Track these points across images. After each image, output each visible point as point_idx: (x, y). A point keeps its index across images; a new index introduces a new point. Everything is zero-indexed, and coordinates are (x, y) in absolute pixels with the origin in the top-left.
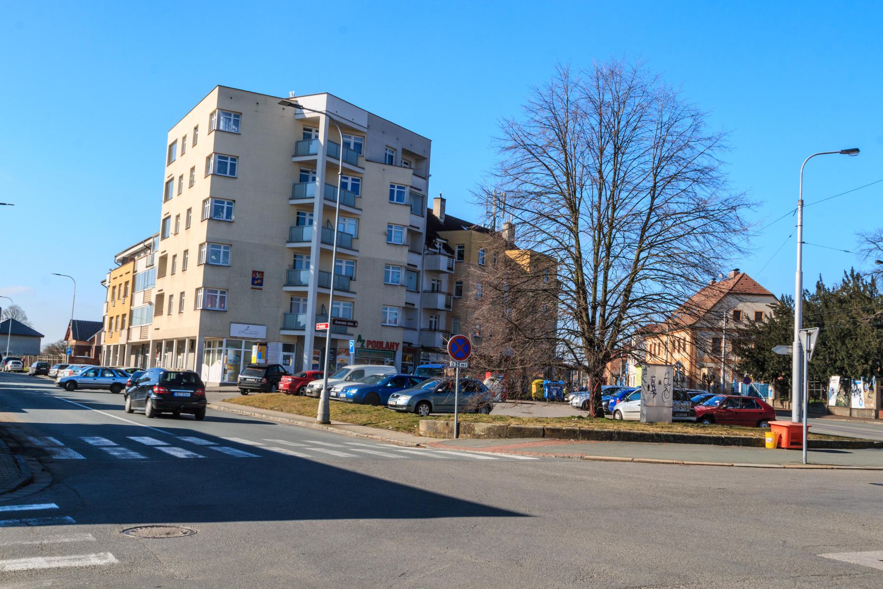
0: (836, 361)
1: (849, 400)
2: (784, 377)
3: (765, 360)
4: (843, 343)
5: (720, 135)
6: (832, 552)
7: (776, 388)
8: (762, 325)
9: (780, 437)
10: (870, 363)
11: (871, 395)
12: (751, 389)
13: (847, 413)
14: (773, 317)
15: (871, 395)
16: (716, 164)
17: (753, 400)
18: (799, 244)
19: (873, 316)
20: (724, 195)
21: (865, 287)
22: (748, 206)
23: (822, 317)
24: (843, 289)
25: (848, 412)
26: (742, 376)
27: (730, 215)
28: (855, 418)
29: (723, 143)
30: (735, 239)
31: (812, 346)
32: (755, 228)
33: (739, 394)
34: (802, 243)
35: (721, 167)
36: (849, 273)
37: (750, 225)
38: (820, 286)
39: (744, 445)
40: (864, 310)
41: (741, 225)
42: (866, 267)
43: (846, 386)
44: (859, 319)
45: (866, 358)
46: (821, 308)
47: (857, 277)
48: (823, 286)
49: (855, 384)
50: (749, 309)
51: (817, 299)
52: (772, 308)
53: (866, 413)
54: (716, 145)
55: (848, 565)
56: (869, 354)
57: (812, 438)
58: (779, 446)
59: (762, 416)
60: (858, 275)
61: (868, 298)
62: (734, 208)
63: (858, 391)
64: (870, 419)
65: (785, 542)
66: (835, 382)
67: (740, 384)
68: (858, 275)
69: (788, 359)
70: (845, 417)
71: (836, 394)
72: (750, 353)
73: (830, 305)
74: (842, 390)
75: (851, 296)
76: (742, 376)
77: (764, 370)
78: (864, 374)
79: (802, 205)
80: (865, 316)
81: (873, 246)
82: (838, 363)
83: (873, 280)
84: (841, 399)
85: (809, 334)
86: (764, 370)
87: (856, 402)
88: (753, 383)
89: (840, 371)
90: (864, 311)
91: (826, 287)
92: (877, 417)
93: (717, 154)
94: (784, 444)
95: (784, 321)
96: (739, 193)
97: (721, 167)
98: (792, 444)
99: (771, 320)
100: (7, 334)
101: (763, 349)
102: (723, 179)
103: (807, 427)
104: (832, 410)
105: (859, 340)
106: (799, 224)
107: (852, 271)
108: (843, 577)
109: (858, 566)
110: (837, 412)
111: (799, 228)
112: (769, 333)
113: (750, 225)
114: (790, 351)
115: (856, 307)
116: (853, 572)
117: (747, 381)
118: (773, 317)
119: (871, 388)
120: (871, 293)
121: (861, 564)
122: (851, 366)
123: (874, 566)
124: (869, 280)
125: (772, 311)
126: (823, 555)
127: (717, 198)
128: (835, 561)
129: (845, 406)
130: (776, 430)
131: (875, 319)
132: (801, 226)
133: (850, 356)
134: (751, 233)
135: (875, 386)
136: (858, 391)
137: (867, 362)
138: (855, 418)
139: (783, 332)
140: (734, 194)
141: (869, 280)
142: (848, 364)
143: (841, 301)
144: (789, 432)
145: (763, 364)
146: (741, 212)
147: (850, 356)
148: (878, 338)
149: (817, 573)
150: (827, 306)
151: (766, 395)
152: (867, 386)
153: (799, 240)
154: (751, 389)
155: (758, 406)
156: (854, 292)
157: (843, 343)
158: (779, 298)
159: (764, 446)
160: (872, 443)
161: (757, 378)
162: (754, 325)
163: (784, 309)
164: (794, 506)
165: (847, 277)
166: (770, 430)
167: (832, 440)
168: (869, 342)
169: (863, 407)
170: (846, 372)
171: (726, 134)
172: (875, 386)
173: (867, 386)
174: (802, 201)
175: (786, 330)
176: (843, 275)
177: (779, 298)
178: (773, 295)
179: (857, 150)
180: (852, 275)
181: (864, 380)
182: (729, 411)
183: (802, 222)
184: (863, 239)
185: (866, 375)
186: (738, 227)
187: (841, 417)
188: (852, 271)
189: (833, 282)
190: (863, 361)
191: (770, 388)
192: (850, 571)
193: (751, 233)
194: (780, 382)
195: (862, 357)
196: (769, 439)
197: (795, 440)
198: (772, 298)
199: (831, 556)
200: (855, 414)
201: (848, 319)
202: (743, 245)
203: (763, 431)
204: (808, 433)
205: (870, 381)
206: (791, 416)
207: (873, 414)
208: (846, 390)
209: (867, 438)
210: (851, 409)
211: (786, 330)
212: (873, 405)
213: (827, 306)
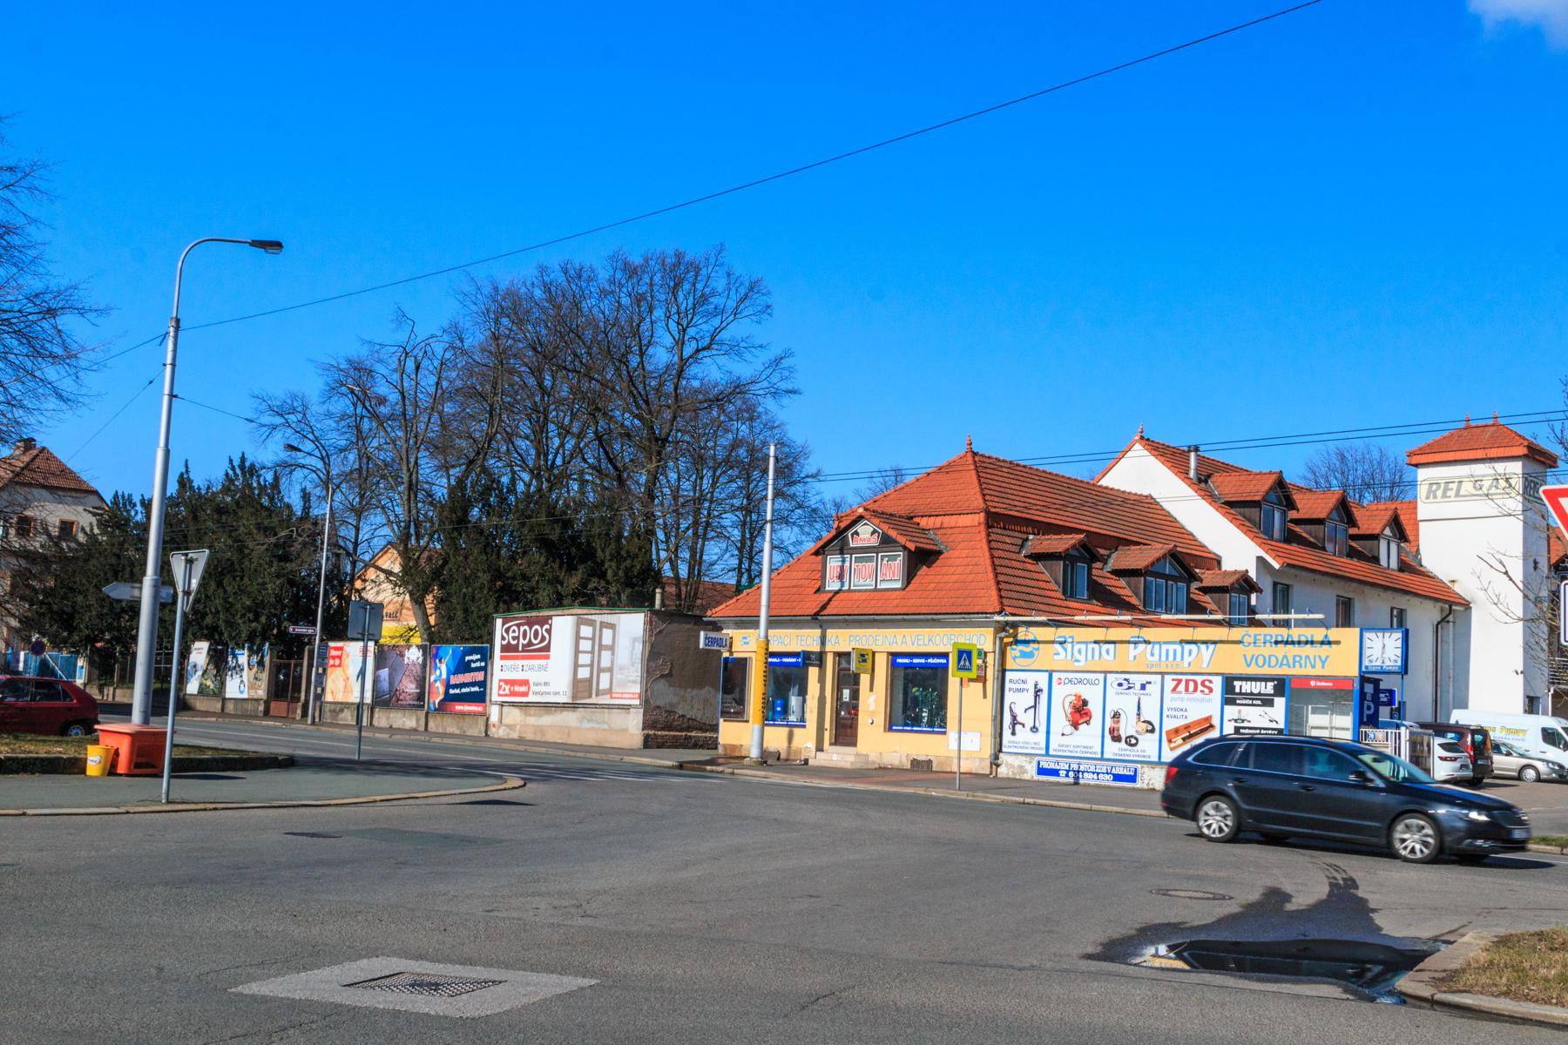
0: (204, 615)
1: (223, 684)
2: (108, 641)
3: (75, 611)
4: (220, 584)
5: (33, 166)
6: (254, 979)
7: (91, 663)
8: (73, 545)
9: (117, 753)
10: (263, 619)
11: (260, 675)
12: (44, 667)
13: (216, 706)
14: (96, 531)
15: (260, 675)
16: (21, 221)
17: (47, 683)
18: (166, 399)
19: (273, 540)
20: (36, 285)
21: (262, 488)
22: (82, 312)
23: (185, 536)
24: (226, 489)
25: (219, 706)
26: (27, 640)
27: (45, 324)
28: (230, 716)
29: (43, 185)
30: (51, 372)
31: (195, 583)
32: (92, 356)
33: (19, 673)
34: (172, 396)
35: (31, 229)
36: (236, 463)
37: (83, 349)
38: (184, 482)
39: (44, 772)
40: (259, 527)
41: (65, 348)
42: (267, 454)
43: (219, 662)
44: (251, 545)
45: (256, 610)
46: (191, 516)
47: (250, 471)
48: (191, 482)
49: (235, 656)
50: (52, 513)
51: (178, 505)
52: (95, 515)
53: (250, 706)
54: (23, 183)
55: (292, 1005)
56: (262, 605)
57: (181, 754)
58: (111, 770)
59: (81, 717)
60: (252, 465)
61: (267, 509)
62: (51, 312)
63: (238, 668)
64: (256, 717)
65: (160, 969)
66: (200, 653)
67: (22, 654)
68: (252, 465)
69: (134, 609)
70: (213, 714)
71: (200, 673)
72: (46, 596)
73: (201, 514)
74: (211, 667)
75: (237, 503)
76: (27, 640)
77: (71, 629)
78: (251, 639)
79: (177, 329)
80: (260, 538)
81: (278, 420)
82: (209, 620)
83: (276, 478)
84: (209, 683)
85: (190, 562)
86: (71, 629)
87: (235, 688)
88: (46, 655)
89: (211, 634)
90: (259, 529)
91: (195, 485)
92: (267, 712)
93: (24, 202)
94: (122, 767)
95: (115, 541)
96: (65, 283)
97: (31, 229)
98: (138, 766)
99: (91, 537)
100: (160, 775)
101: (72, 590)
102: (32, 253)
103: (173, 732)
104: (191, 701)
105: (246, 580)
106: (169, 361)
107: (243, 459)
108: (291, 1032)
109: (310, 1003)
110: (200, 705)
111: (169, 368)
112: (86, 561)
113: (83, 349)
114: (136, 593)
115: (246, 522)
116: (304, 1018)
117: (37, 649)
118: (96, 531)
119: (261, 663)
120: (272, 499)
121: (315, 998)
122: (230, 624)
123: (338, 999)
124: (269, 477)
125: (94, 520)
126: (240, 988)
127: (19, 287)
128: (265, 1000)
129: (215, 694)
130: (109, 742)
131: (276, 545)
132: (173, 365)
133: (228, 608)
134: (83, 364)
135: (267, 659)
136: (238, 668)
137: (257, 619)
138: (230, 716)
139: (113, 561)
140: (53, 284)
141: (269, 477)
142: (226, 622)
143: (221, 510)
144: (132, 745)
145: (71, 616)
146: (66, 321)
147: (228, 608)
148: (278, 577)
149: (239, 1031)
150: (195, 518)
151: (72, 672)
152: (255, 659)
153: (167, 391)
154: (44, 663)
155: (66, 695)
156: (243, 497)
157: (220, 584)
158: (108, 498)
159: (83, 771)
160: (276, 759)
161: (57, 644)
162: (57, 544)
163: (119, 520)
164: (159, 889)
165: (233, 468)
166: (96, 742)
167: (208, 755)
168: (265, 583)
169: (245, 696)
170: (221, 634)
171: (45, 166)
172: (267, 659)
173: (255, 659)
174: (178, 321)
175: (118, 556)
176: (227, 465)
177: (108, 498)
178: (95, 493)
179: (278, 245)
180: (242, 466)
181: (250, 649)
182: (11, 705)
183: (174, 358)
184: (264, 407)
185: (253, 643)
186: (58, 350)
187: (207, 714)
188: (243, 459)
189: (209, 474)
190: (251, 616)
191: (81, 662)
192: (296, 1013)
193: (83, 364)
194: (99, 650)
195: (249, 609)
196: (94, 758)
197: (145, 758)
198: (93, 498)
199: (255, 988)
200: (230, 707)
201: (230, 542)
202: (67, 385)
203: (82, 744)
204: (174, 746)
205: (260, 650)
206: (130, 714)
207: (261, 708)
208: (217, 667)
209: (282, 751)
210: (224, 700)
211: (118, 556)
212: (261, 693)
213: (195, 518)
